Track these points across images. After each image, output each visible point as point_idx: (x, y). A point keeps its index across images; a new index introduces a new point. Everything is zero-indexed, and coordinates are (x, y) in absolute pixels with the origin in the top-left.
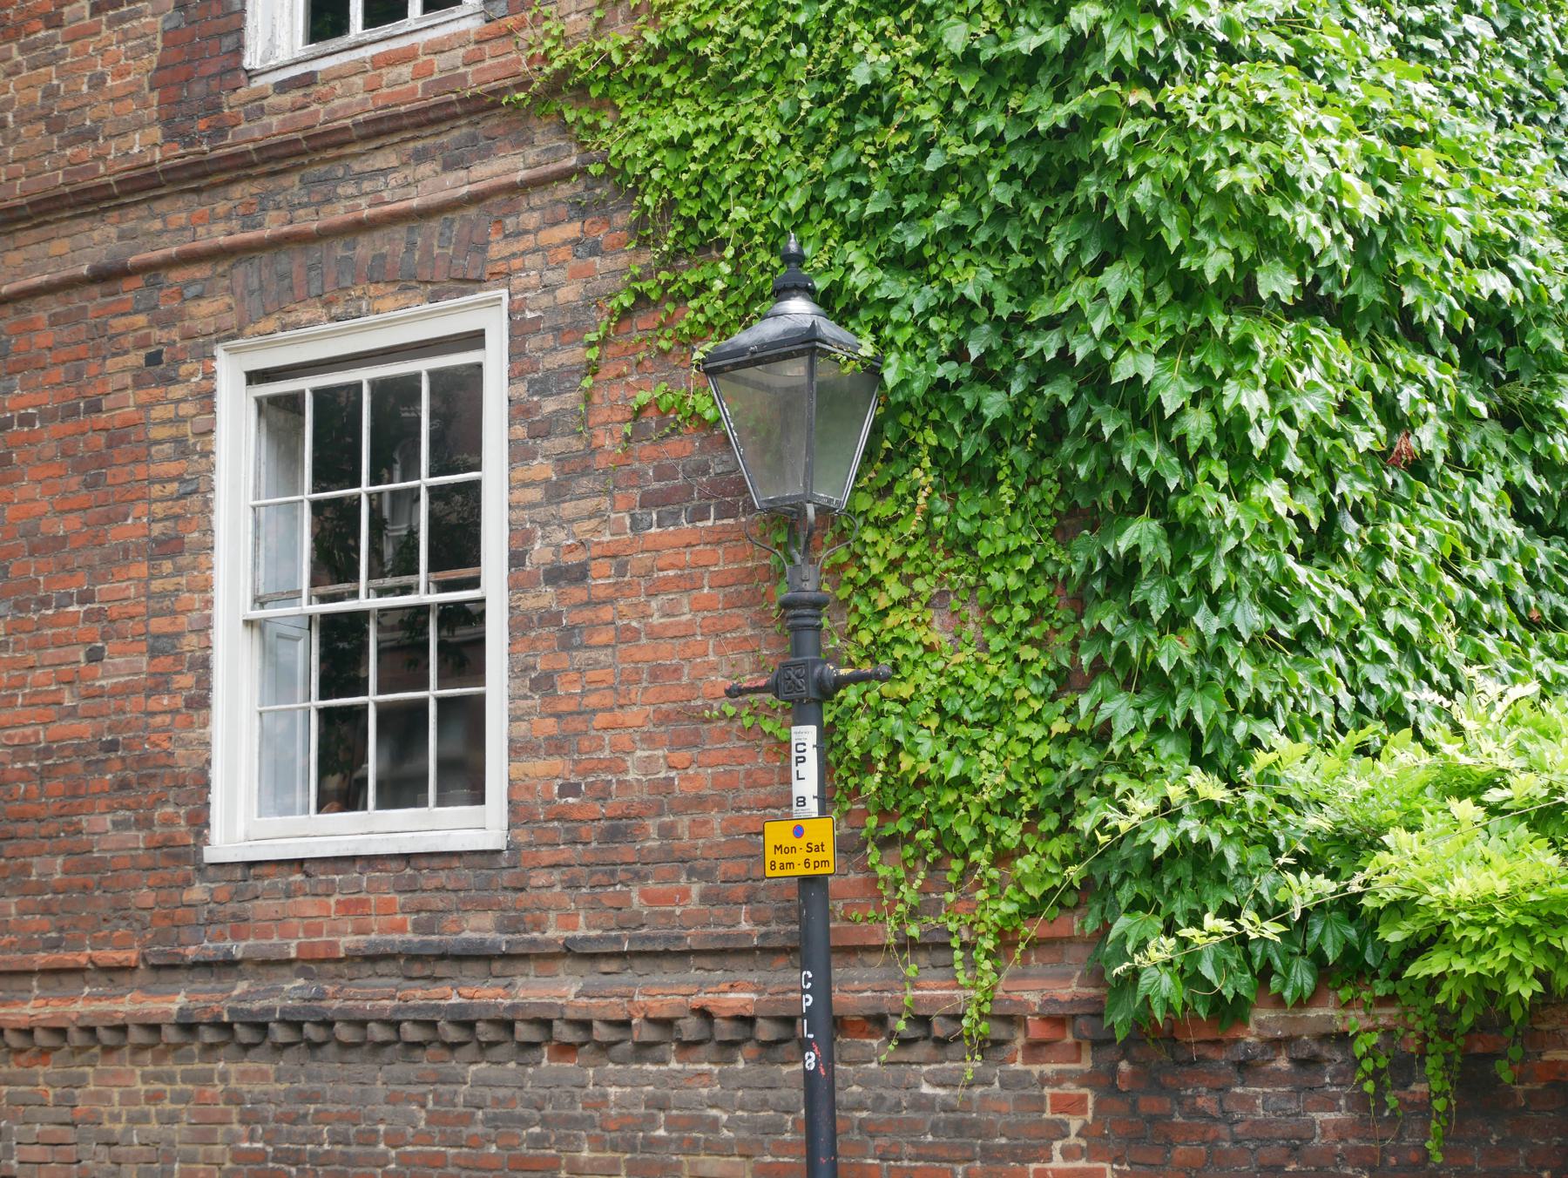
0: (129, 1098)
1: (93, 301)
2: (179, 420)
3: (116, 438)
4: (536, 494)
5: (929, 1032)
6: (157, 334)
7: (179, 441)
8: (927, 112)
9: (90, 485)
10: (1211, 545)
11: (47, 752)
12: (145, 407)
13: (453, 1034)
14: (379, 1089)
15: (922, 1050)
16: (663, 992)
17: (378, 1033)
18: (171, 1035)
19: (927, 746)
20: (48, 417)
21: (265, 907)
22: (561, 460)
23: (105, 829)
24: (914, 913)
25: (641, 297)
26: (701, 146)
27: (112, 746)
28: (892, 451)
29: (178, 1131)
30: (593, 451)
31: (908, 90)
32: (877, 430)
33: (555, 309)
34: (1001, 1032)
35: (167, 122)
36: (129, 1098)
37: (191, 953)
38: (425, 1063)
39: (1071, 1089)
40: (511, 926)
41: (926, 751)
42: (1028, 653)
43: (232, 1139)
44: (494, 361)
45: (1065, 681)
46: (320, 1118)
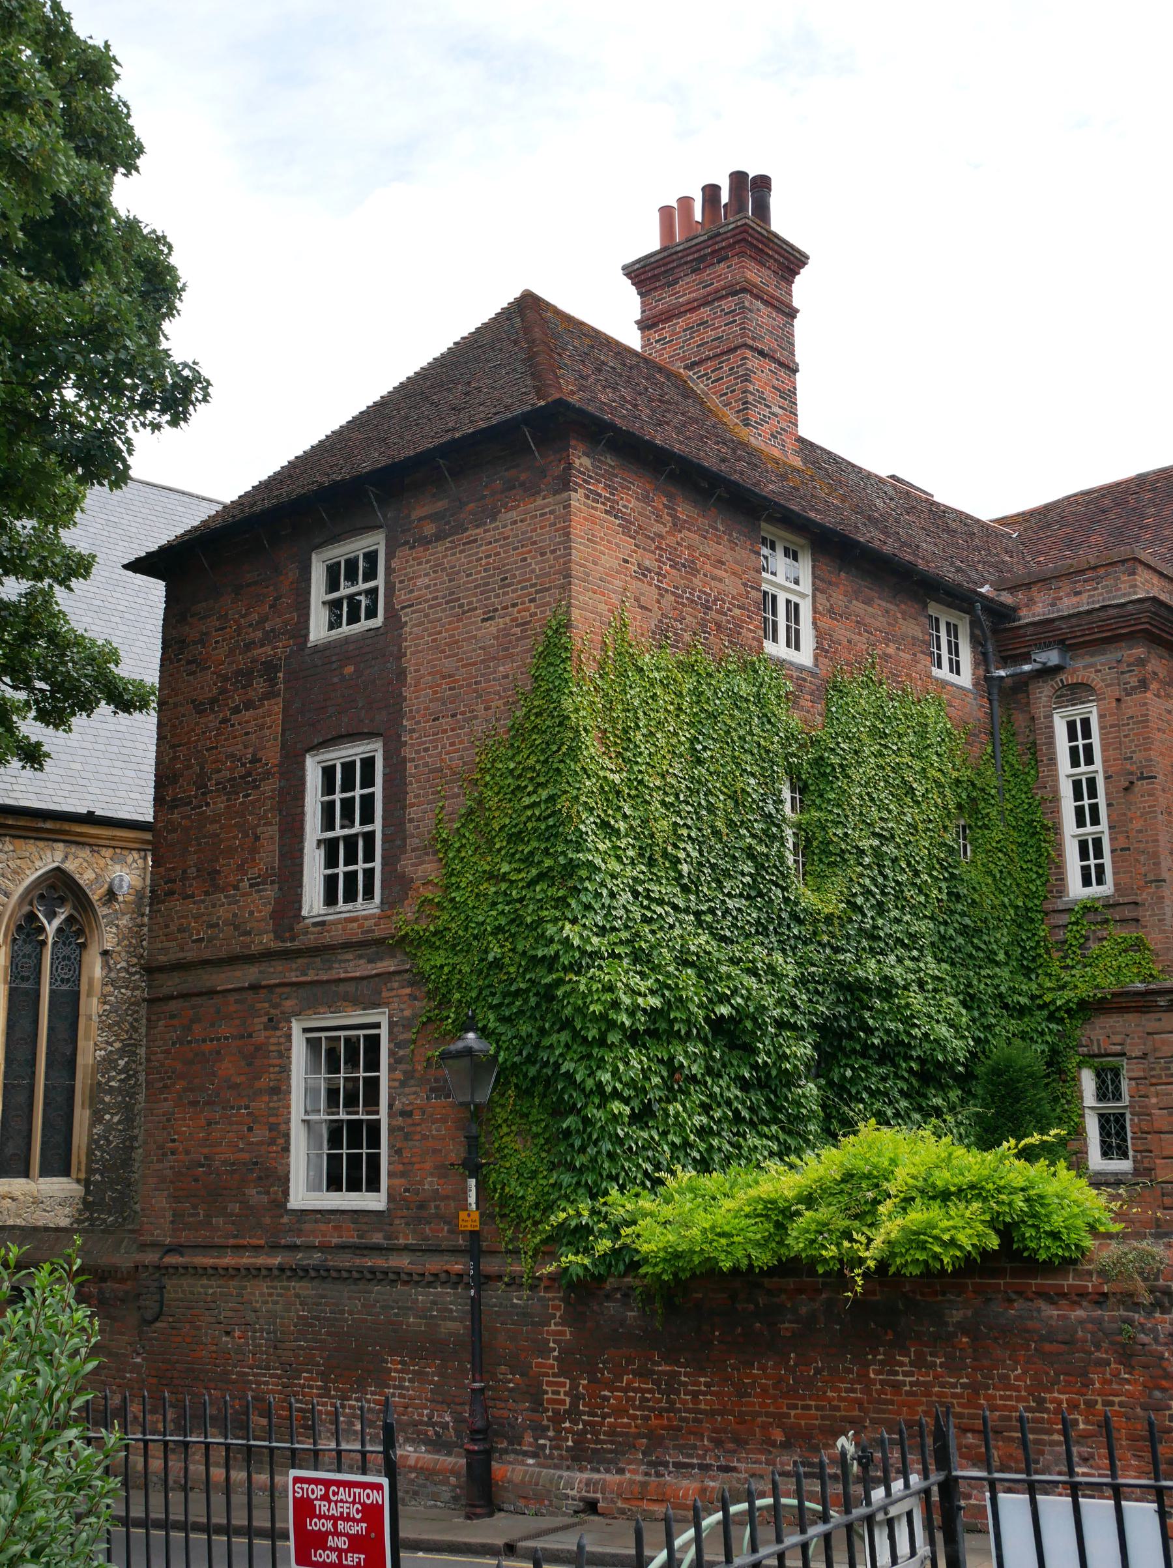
0: (262, 1294)
1: (250, 996)
2: (279, 1044)
3: (258, 1048)
4: (396, 1084)
5: (514, 1282)
6: (272, 1011)
7: (279, 1052)
8: (512, 970)
9: (249, 1065)
10: (593, 1125)
11: (234, 1164)
12: (268, 1038)
13: (369, 1276)
14: (346, 1294)
15: (514, 1287)
16: (434, 1264)
17: (345, 1274)
18: (276, 1272)
19: (513, 1184)
20: (233, 1037)
21: (308, 1226)
22: (405, 1073)
23: (253, 1194)
24: (511, 1240)
25: (429, 1018)
26: (446, 970)
27: (256, 1163)
28: (501, 1084)
29: (279, 1307)
30: (414, 1071)
31: (507, 961)
32: (498, 1074)
33: (402, 1018)
34: (536, 1282)
35: (275, 932)
36: (262, 1294)
37: (283, 1242)
38: (361, 1286)
39: (557, 1302)
40: (388, 1237)
41: (514, 1188)
42: (544, 1155)
43: (297, 1311)
44: (384, 1033)
45: (553, 1167)
46: (326, 1304)
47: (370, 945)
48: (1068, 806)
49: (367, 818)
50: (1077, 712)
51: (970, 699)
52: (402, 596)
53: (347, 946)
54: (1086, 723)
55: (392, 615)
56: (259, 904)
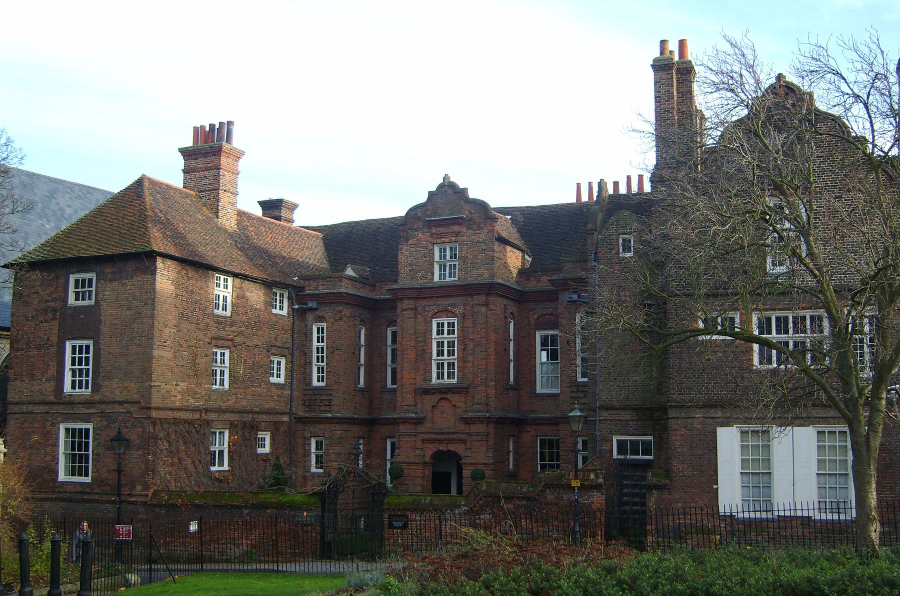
1: (45, 415)
47: (87, 403)
48: (315, 354)
49: (87, 364)
50: (321, 325)
51: (286, 319)
52: (100, 297)
53: (80, 403)
54: (323, 329)
55: (97, 301)
56: (49, 387)
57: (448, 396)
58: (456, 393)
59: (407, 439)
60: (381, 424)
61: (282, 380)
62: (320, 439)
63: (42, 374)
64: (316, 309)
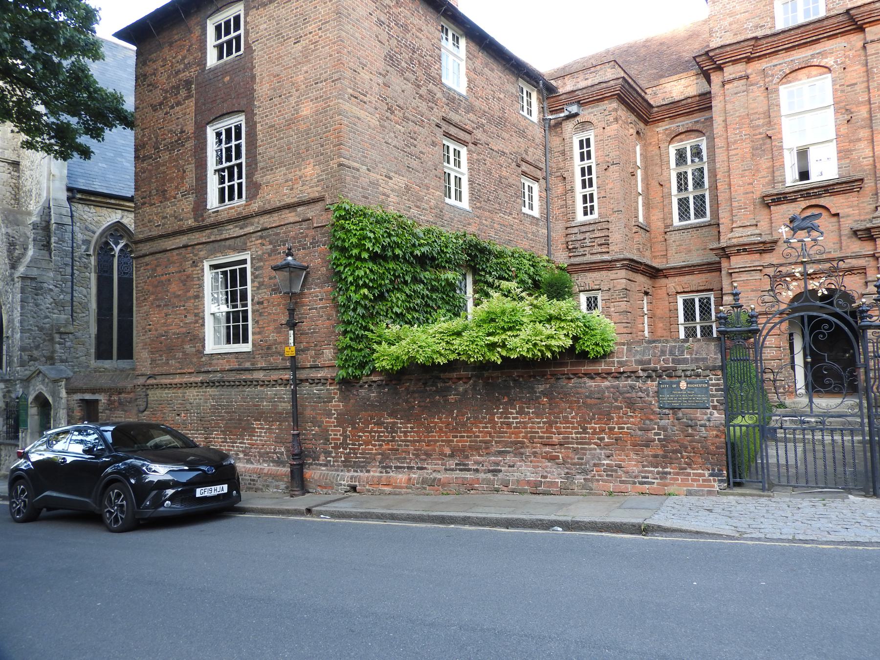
1: (183, 251)
49: (238, 156)
53: (230, 221)
56: (186, 205)
57: (822, 201)
58: (838, 193)
59: (744, 277)
60: (666, 277)
61: (536, 213)
62: (592, 294)
63: (177, 188)
64: (576, 115)
